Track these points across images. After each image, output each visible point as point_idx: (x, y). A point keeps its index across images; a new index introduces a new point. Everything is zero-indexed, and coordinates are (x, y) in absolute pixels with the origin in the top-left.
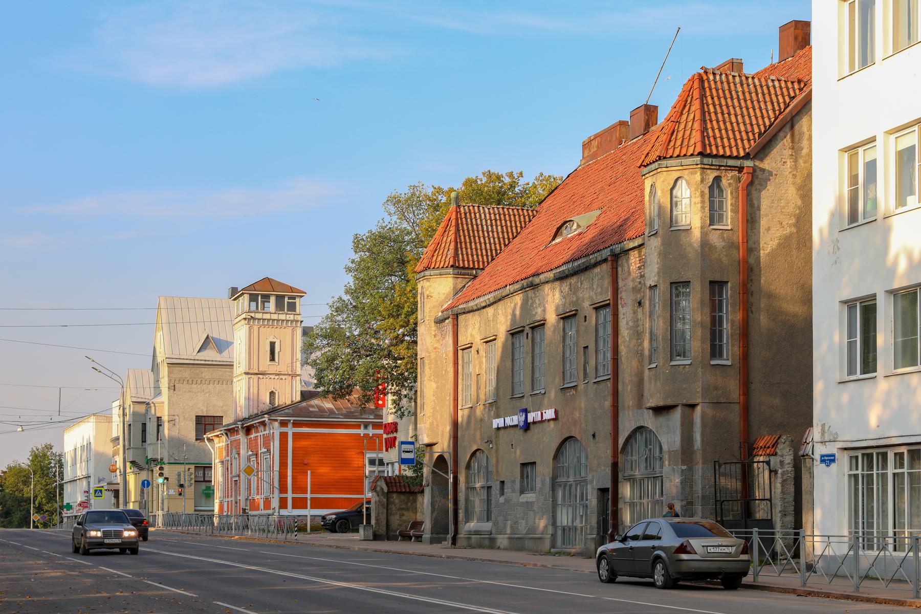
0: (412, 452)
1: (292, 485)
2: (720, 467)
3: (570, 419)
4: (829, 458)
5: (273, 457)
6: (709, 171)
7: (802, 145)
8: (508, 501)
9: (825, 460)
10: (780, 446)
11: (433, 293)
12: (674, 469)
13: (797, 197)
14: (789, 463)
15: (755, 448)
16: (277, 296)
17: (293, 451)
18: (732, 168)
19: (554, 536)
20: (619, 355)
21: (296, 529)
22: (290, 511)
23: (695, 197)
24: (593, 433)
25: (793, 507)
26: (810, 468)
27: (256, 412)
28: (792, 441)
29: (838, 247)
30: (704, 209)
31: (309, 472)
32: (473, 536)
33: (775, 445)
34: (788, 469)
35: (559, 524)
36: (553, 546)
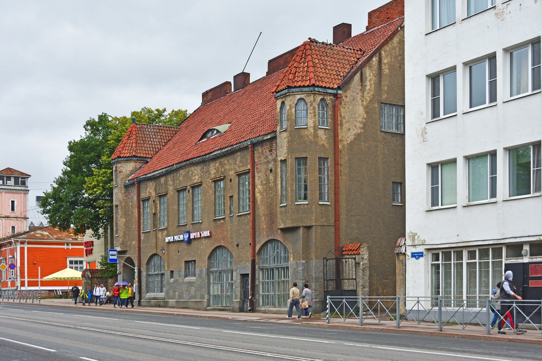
0: (115, 255)
1: (28, 274)
2: (327, 262)
3: (220, 236)
4: (419, 254)
5: (16, 260)
6: (317, 96)
7: (366, 84)
8: (176, 281)
9: (416, 256)
10: (362, 249)
11: (123, 170)
12: (297, 263)
13: (364, 113)
14: (366, 259)
15: (344, 251)
16: (15, 177)
17: (27, 257)
18: (330, 94)
19: (209, 300)
20: (256, 200)
21: (40, 297)
22: (26, 288)
23: (310, 110)
24: (237, 244)
25: (368, 283)
26: (402, 261)
27: (4, 237)
28: (368, 246)
29: (425, 132)
30: (315, 117)
31: (39, 268)
32: (153, 300)
33: (359, 248)
34: (366, 262)
35: (211, 293)
36: (209, 305)
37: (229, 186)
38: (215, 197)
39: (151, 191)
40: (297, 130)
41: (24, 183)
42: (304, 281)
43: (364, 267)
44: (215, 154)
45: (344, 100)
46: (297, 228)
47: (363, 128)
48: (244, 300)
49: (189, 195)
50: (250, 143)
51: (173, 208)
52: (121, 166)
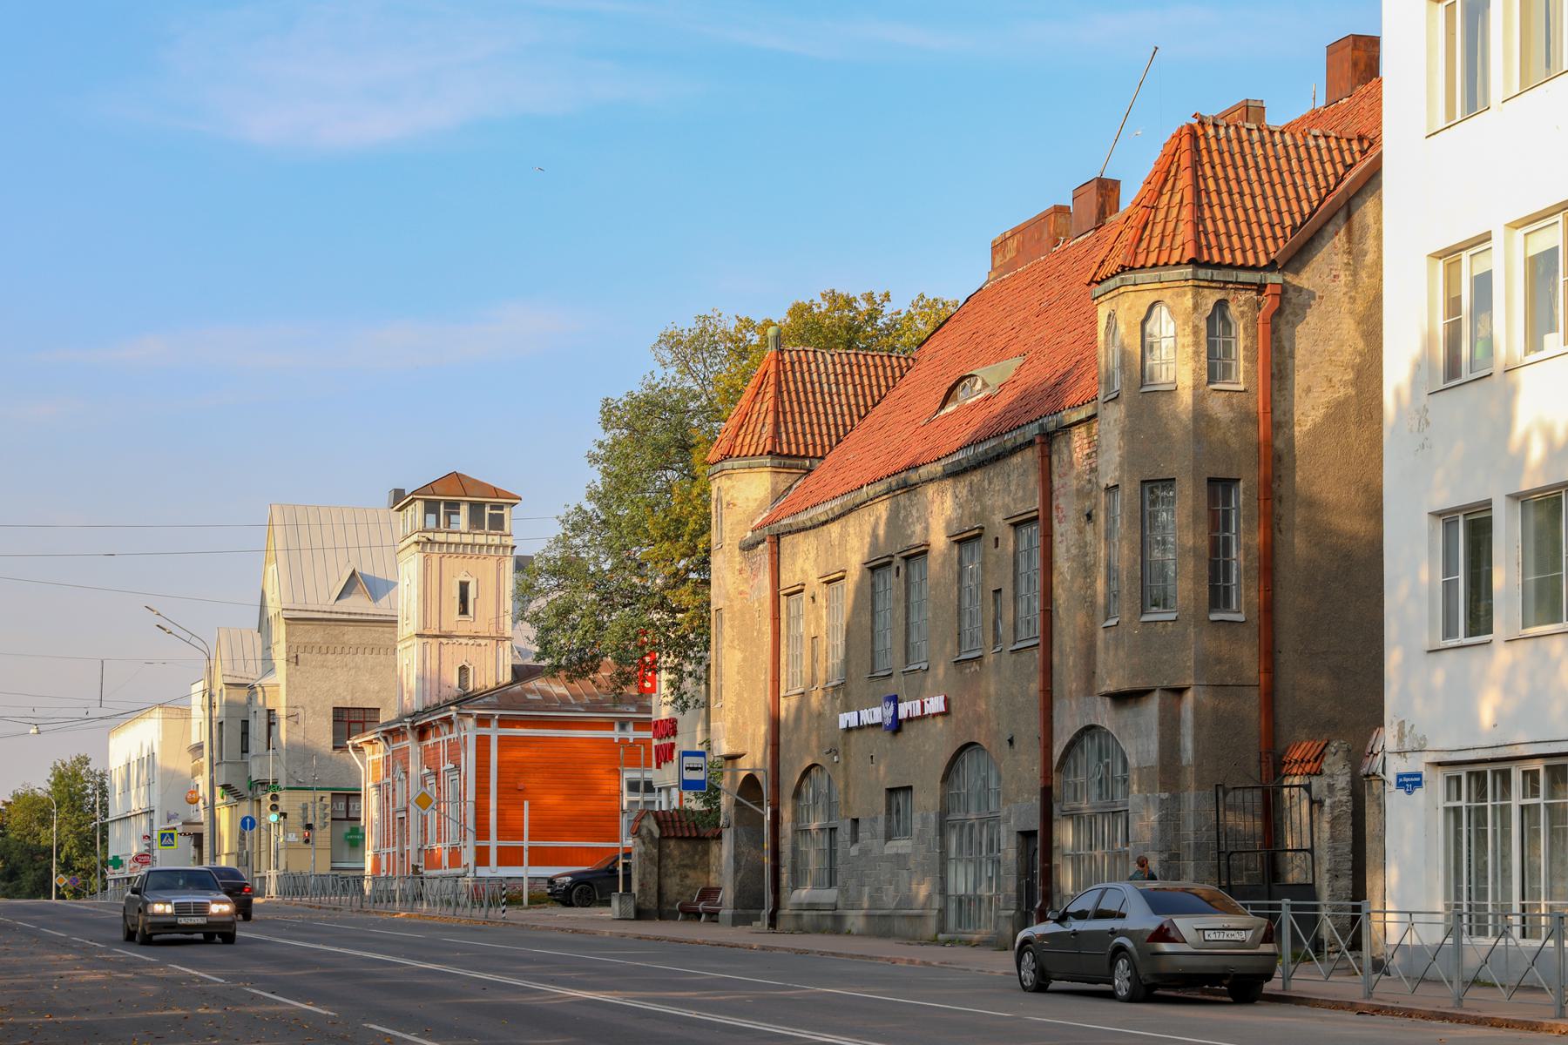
0: (701, 769)
3: (970, 714)
4: (1412, 779)
5: (465, 778)
6: (1206, 292)
7: (1365, 247)
8: (864, 853)
11: (737, 498)
13: (1357, 335)
15: (1285, 763)
16: (472, 504)
18: (1247, 286)
20: (1054, 604)
21: (504, 900)
22: (493, 871)
24: (1009, 737)
25: (1350, 864)
27: (435, 701)
29: (1426, 420)
30: (1199, 356)
34: (1342, 798)
35: (951, 891)
36: (942, 928)
37: (992, 559)
38: (960, 590)
39: (807, 566)
40: (1146, 396)
41: (497, 523)
42: (1165, 856)
43: (1336, 812)
44: (959, 460)
45: (1293, 301)
46: (1146, 692)
47: (1355, 383)
48: (1026, 913)
49: (899, 583)
50: (1037, 432)
51: (860, 622)
52: (733, 487)
